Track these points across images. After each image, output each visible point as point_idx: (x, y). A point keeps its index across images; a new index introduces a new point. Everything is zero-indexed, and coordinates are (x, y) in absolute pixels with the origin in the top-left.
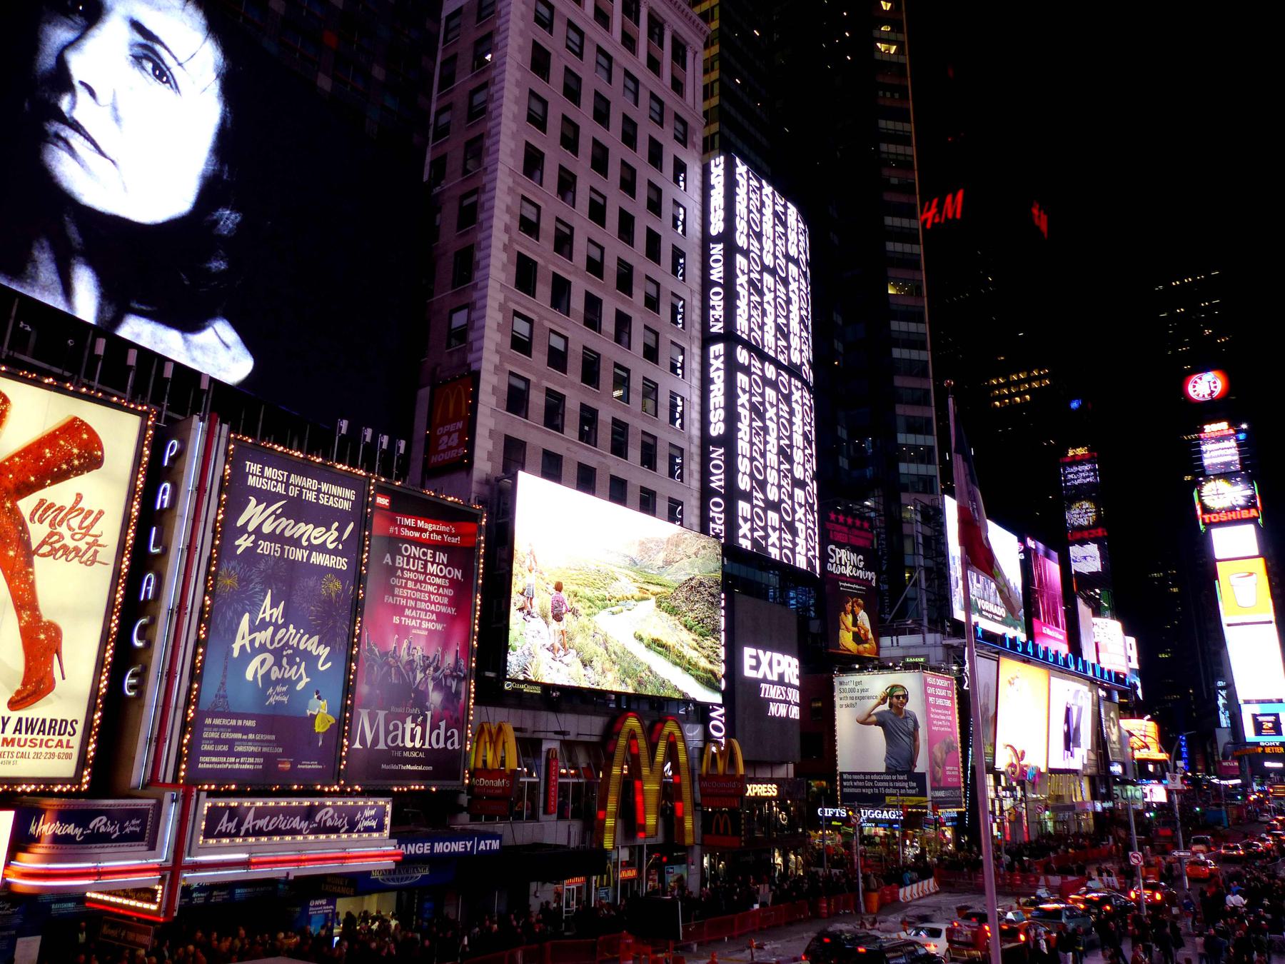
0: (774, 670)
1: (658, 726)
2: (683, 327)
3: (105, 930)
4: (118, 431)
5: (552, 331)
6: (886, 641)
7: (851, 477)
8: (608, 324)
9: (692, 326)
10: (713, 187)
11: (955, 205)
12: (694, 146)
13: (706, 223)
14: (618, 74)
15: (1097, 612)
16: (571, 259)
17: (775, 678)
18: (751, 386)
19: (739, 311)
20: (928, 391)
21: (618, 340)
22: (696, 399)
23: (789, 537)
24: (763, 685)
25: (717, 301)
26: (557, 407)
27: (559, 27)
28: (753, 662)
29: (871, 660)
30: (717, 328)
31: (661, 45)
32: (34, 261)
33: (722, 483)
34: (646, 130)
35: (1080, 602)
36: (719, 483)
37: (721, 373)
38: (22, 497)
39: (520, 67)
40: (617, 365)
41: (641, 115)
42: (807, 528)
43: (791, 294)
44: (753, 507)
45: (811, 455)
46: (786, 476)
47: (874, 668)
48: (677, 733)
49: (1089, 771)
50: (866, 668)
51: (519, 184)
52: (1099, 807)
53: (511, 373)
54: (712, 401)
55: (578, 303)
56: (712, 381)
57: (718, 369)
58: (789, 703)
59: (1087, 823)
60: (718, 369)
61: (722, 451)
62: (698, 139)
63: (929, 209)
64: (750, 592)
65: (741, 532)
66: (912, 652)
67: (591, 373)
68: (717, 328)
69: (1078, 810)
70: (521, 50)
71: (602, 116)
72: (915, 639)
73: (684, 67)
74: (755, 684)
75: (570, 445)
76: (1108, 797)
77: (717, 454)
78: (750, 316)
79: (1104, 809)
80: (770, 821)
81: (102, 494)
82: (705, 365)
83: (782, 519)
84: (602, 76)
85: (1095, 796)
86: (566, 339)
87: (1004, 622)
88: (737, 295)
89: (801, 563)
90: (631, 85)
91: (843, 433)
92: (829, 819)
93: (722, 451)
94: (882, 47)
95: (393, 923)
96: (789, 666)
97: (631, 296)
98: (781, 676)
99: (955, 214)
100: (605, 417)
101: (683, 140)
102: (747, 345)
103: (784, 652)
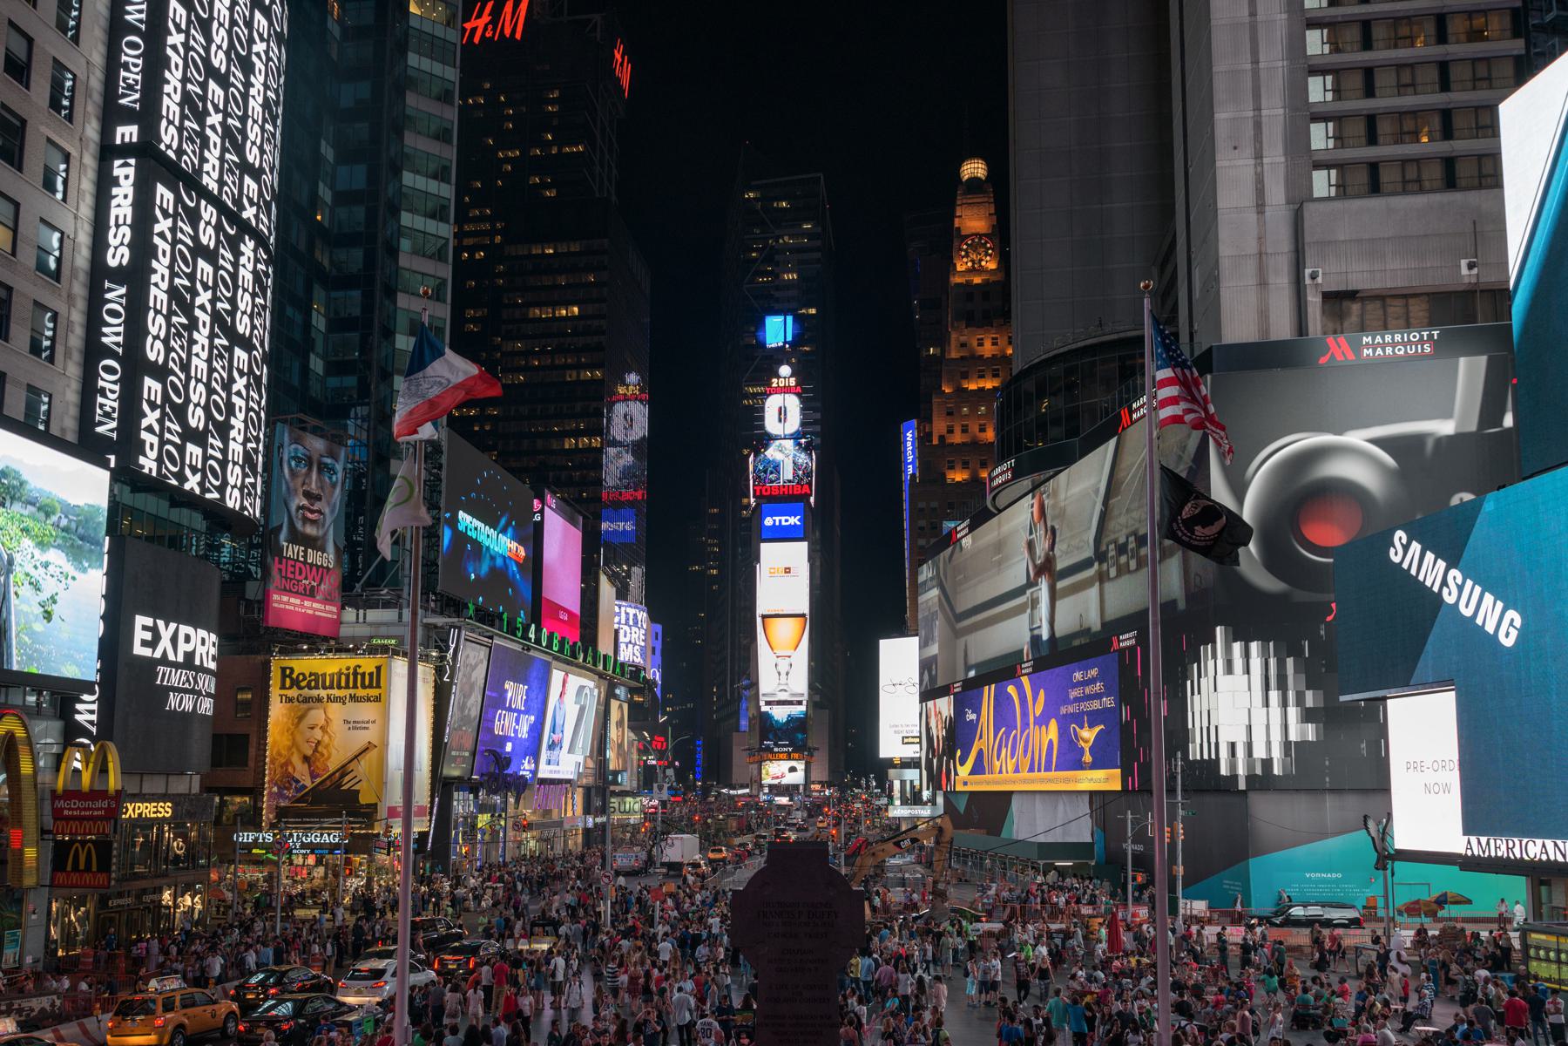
0: (186, 646)
2: (64, 199)
6: (350, 614)
7: (322, 374)
15: (622, 594)
17: (180, 659)
19: (167, 89)
20: (444, 281)
22: (77, 317)
24: (161, 669)
28: (148, 636)
29: (326, 639)
33: (120, 339)
35: (603, 579)
36: (138, 16)
42: (249, 409)
45: (264, 307)
46: (221, 356)
47: (330, 651)
48: (20, 733)
49: (585, 781)
50: (318, 650)
52: (590, 821)
54: (114, 212)
58: (199, 693)
59: (576, 843)
61: (123, 291)
63: (479, 16)
65: (145, 423)
66: (383, 630)
68: (130, 100)
69: (567, 826)
72: (389, 615)
74: (151, 664)
77: (116, 295)
79: (596, 824)
80: (155, 850)
85: (587, 810)
89: (233, 501)
92: (248, 847)
93: (123, 291)
96: (203, 644)
98: (189, 656)
99: (514, 31)
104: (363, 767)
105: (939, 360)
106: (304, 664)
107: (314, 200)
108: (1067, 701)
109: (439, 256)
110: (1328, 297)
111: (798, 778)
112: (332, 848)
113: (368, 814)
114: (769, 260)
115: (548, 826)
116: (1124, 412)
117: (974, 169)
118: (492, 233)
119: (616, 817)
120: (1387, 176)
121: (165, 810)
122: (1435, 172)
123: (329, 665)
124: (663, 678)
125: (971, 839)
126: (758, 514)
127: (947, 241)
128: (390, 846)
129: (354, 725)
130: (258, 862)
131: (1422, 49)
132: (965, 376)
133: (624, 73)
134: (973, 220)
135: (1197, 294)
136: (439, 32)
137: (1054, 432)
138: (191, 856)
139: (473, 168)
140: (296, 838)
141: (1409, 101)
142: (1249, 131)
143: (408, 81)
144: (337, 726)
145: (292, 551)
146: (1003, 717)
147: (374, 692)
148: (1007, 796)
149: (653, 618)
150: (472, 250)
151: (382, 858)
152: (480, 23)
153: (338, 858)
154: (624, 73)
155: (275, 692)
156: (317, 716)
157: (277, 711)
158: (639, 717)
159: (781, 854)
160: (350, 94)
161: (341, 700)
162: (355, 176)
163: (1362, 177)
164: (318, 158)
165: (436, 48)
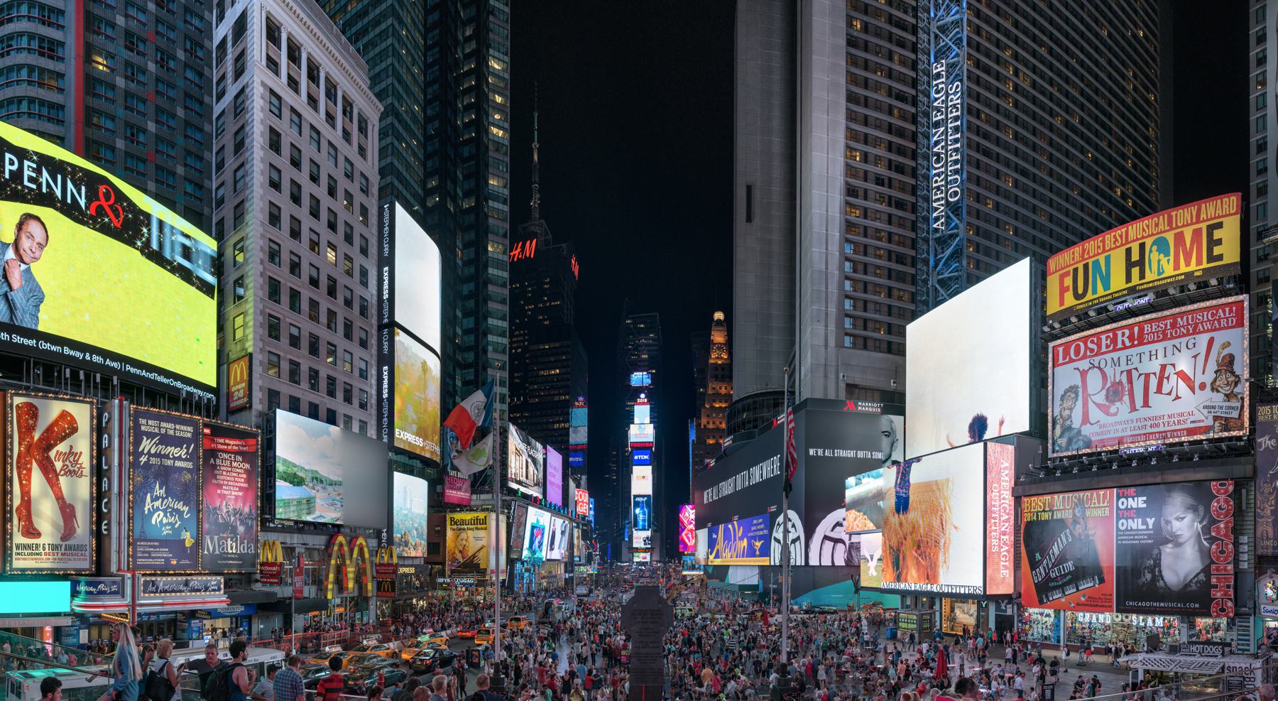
4: (81, 413)
6: (474, 497)
31: (351, 120)
34: (343, 184)
40: (329, 343)
59: (562, 584)
62: (375, 190)
72: (489, 496)
73: (366, 137)
80: (409, 584)
81: (82, 444)
94: (495, 130)
100: (323, 374)
101: (365, 191)
104: (481, 555)
105: (704, 394)
106: (458, 516)
107: (455, 334)
108: (750, 531)
109: (504, 352)
110: (848, 386)
111: (648, 559)
112: (471, 585)
113: (484, 572)
114: (636, 349)
115: (551, 576)
117: (719, 316)
118: (523, 341)
120: (870, 343)
121: (412, 570)
122: (885, 346)
123: (467, 516)
124: (595, 516)
125: (713, 583)
126: (632, 454)
127: (708, 345)
128: (492, 584)
129: (477, 539)
130: (445, 589)
131: (882, 298)
133: (576, 270)
134: (718, 337)
136: (500, 257)
137: (747, 426)
138: (422, 586)
139: (516, 314)
140: (458, 581)
141: (877, 316)
142: (823, 315)
143: (488, 281)
144: (471, 539)
145: (453, 473)
146: (727, 537)
148: (728, 566)
149: (590, 496)
150: (516, 348)
151: (489, 589)
152: (516, 252)
153: (474, 588)
154: (576, 270)
155: (448, 527)
156: (464, 535)
157: (449, 533)
158: (585, 536)
159: (640, 590)
160: (467, 289)
162: (470, 323)
163: (861, 342)
164: (455, 316)
165: (499, 265)
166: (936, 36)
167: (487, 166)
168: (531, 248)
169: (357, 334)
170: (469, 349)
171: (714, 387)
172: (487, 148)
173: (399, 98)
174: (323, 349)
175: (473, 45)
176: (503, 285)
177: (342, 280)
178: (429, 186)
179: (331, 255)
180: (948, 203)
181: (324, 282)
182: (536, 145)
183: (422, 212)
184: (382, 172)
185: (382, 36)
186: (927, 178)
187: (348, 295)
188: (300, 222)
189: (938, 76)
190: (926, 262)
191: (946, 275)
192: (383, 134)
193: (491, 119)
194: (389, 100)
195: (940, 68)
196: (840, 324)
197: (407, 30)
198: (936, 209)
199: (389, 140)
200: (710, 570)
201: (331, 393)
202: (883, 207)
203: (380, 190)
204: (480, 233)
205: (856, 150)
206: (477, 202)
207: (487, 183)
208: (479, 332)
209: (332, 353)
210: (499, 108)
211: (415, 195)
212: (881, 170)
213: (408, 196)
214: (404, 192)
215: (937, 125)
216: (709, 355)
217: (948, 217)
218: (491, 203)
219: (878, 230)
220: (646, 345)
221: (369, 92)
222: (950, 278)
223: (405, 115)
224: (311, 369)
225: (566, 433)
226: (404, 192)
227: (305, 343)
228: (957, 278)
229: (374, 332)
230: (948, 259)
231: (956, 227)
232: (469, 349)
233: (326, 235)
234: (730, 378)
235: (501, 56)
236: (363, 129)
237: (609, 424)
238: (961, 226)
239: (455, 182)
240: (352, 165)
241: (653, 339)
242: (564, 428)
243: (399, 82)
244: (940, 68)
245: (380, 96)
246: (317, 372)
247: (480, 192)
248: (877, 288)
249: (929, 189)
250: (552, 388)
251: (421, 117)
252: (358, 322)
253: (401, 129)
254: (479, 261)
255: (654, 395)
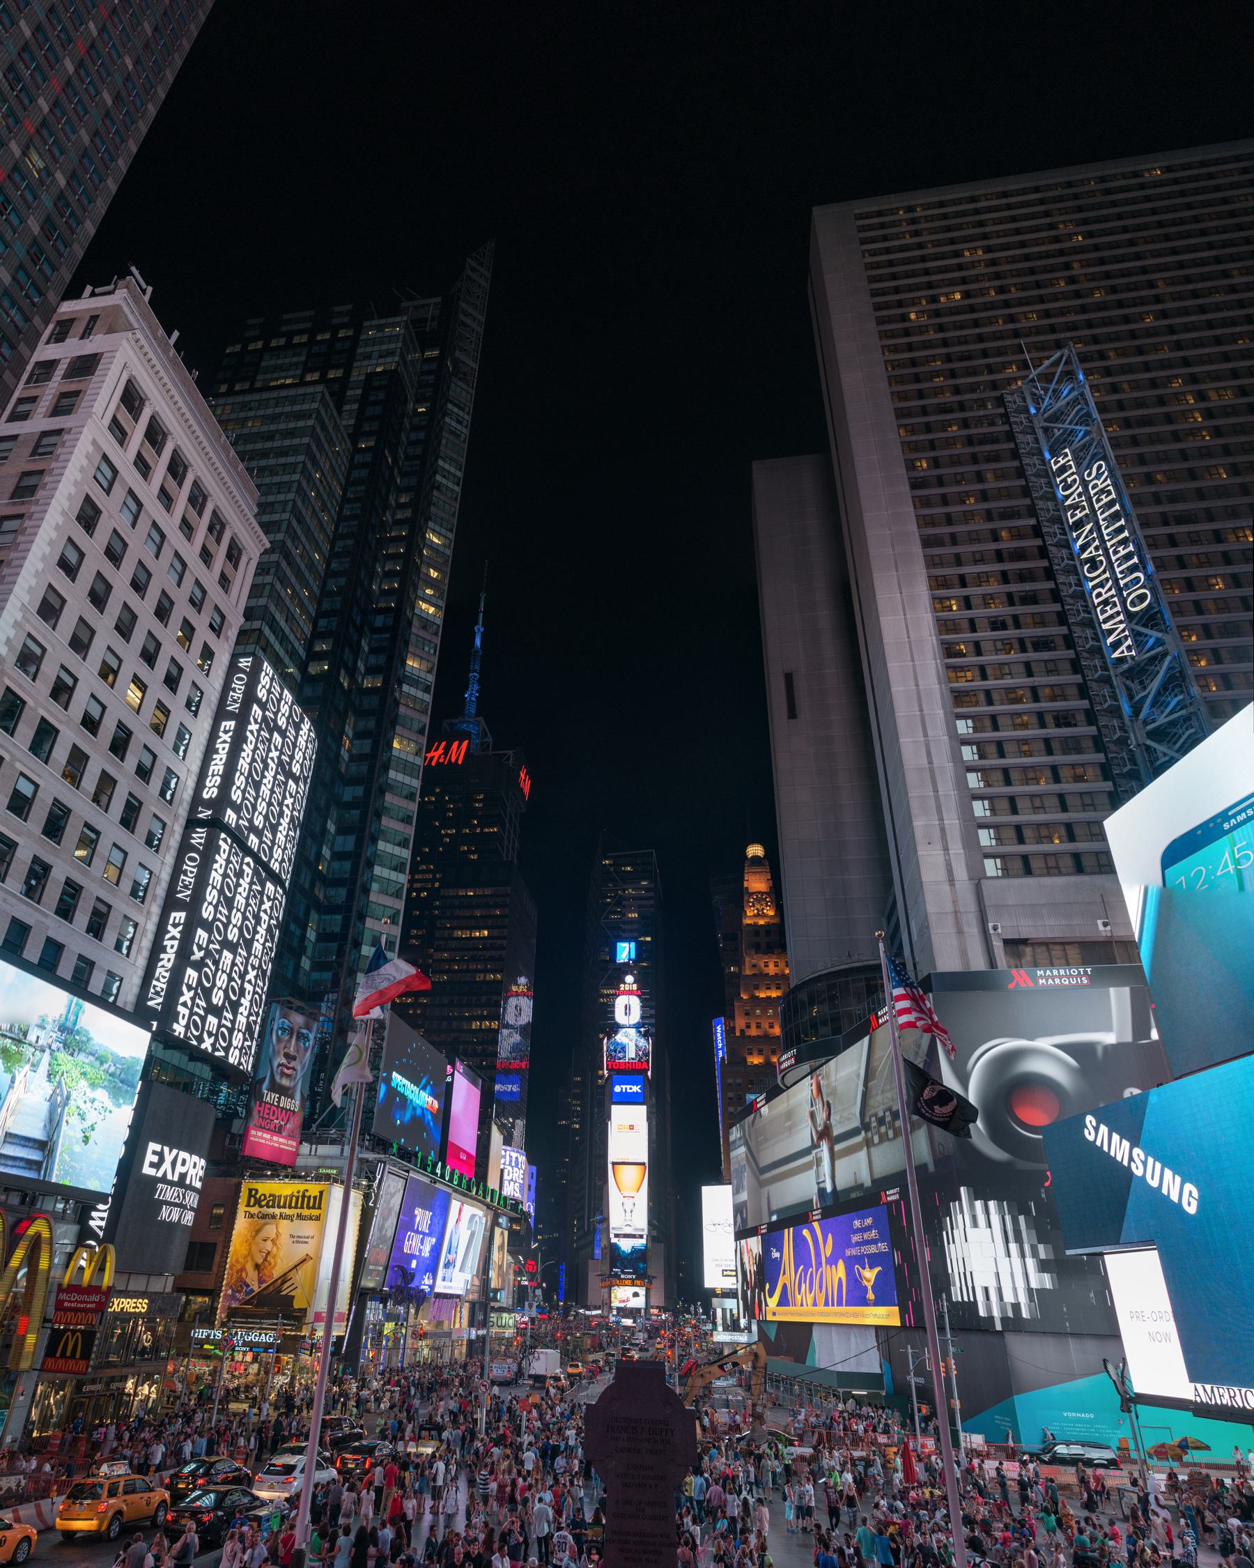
1: (23, 1224)
3: (438, 478)
5: (22, 774)
6: (305, 1148)
7: (309, 970)
8: (90, 781)
9: (180, 804)
10: (216, 751)
11: (176, 334)
12: (227, 639)
13: (200, 784)
14: (167, 552)
16: (66, 708)
18: (214, 976)
21: (96, 799)
23: (225, 912)
24: (160, 1186)
25: (190, 867)
26: (60, 818)
27: (208, 608)
28: (155, 1159)
29: (285, 1167)
30: (233, 708)
31: (218, 541)
32: (646, 1035)
33: (103, 1224)
34: (182, 609)
35: (494, 1128)
37: (176, 943)
38: (23, 949)
39: (64, 513)
40: (87, 825)
41: (180, 597)
42: (255, 993)
43: (246, 985)
44: (261, 842)
51: (28, 621)
53: (29, 635)
55: (61, 753)
56: (163, 950)
57: (173, 938)
60: (173, 938)
62: (233, 633)
64: (181, 1092)
65: (182, 1000)
66: (328, 1162)
67: (54, 827)
69: (454, 1337)
70: (31, 590)
71: (139, 586)
72: (333, 1150)
73: (236, 567)
75: (9, 898)
76: (484, 1324)
78: (256, 748)
80: (128, 1341)
82: (161, 930)
83: (200, 982)
84: (127, 518)
85: (471, 1324)
86: (37, 786)
87: (429, 1543)
88: (245, 740)
90: (179, 567)
91: (331, 827)
92: (201, 1342)
93: (92, 1223)
94: (424, 606)
95: (625, 951)
96: (193, 1167)
97: (122, 759)
98: (183, 1176)
100: (59, 875)
101: (217, 629)
102: (247, 851)
103: (191, 1152)
105: (738, 976)
106: (266, 1187)
108: (850, 1245)
109: (397, 894)
110: (1007, 942)
116: (872, 1017)
117: (755, 850)
119: (494, 1330)
120: (1036, 864)
121: (142, 1305)
126: (610, 1082)
127: (739, 896)
129: (297, 1239)
130: (207, 1357)
131: (1044, 786)
132: (757, 987)
134: (757, 883)
135: (915, 938)
136: (411, 758)
138: (155, 1349)
139: (425, 839)
141: (1041, 817)
142: (937, 833)
144: (284, 1240)
145: (270, 1097)
146: (801, 1257)
147: (315, 1212)
148: (811, 1324)
150: (419, 891)
152: (436, 754)
155: (242, 1208)
156: (270, 1230)
157: (241, 1224)
158: (516, 1243)
161: (290, 1218)
163: (1019, 864)
164: (324, 830)
165: (406, 768)
166: (1046, 430)
167: (407, 643)
168: (458, 751)
169: (144, 823)
170: (337, 882)
171: (754, 963)
172: (410, 623)
173: (295, 537)
174: (72, 831)
175: (408, 513)
176: (411, 797)
177: (142, 735)
178: (317, 648)
179: (134, 695)
180: (1130, 616)
181: (108, 729)
182: (479, 628)
183: (298, 677)
184: (249, 614)
185: (289, 468)
186: (1082, 596)
187: (147, 761)
188: (93, 632)
189: (1063, 469)
190: (1116, 711)
191: (1162, 720)
192: (262, 569)
193: (420, 593)
194: (280, 536)
195: (1066, 458)
196: (970, 842)
197: (323, 474)
198: (1111, 632)
199: (268, 579)
200: (772, 1334)
201: (65, 911)
202: (1014, 656)
203: (242, 633)
204: (381, 719)
205: (949, 599)
206: (386, 682)
207: (404, 663)
208: (359, 860)
209: (85, 842)
210: (431, 583)
211: (292, 653)
212: (999, 610)
213: (282, 653)
214: (277, 646)
215: (1079, 525)
216: (741, 913)
217: (1136, 635)
218: (405, 688)
219: (1009, 690)
220: (635, 898)
221: (253, 520)
222: (1172, 724)
223: (298, 559)
224: (36, 860)
225: (491, 1038)
226: (277, 646)
227: (39, 813)
228: (1187, 719)
229: (178, 829)
230: (1159, 693)
231: (1159, 642)
232: (337, 882)
233: (132, 664)
234: (783, 947)
235: (443, 531)
236: (234, 554)
237: (572, 1026)
238: (1167, 638)
239: (356, 651)
240: (204, 592)
241: (647, 889)
242: (490, 1030)
243: (299, 522)
244: (1066, 458)
245: (267, 527)
246: (47, 868)
247: (391, 670)
248: (1030, 773)
249: (1089, 609)
250: (474, 959)
251: (321, 568)
252: (152, 805)
253: (289, 572)
254: (376, 759)
255: (646, 969)
